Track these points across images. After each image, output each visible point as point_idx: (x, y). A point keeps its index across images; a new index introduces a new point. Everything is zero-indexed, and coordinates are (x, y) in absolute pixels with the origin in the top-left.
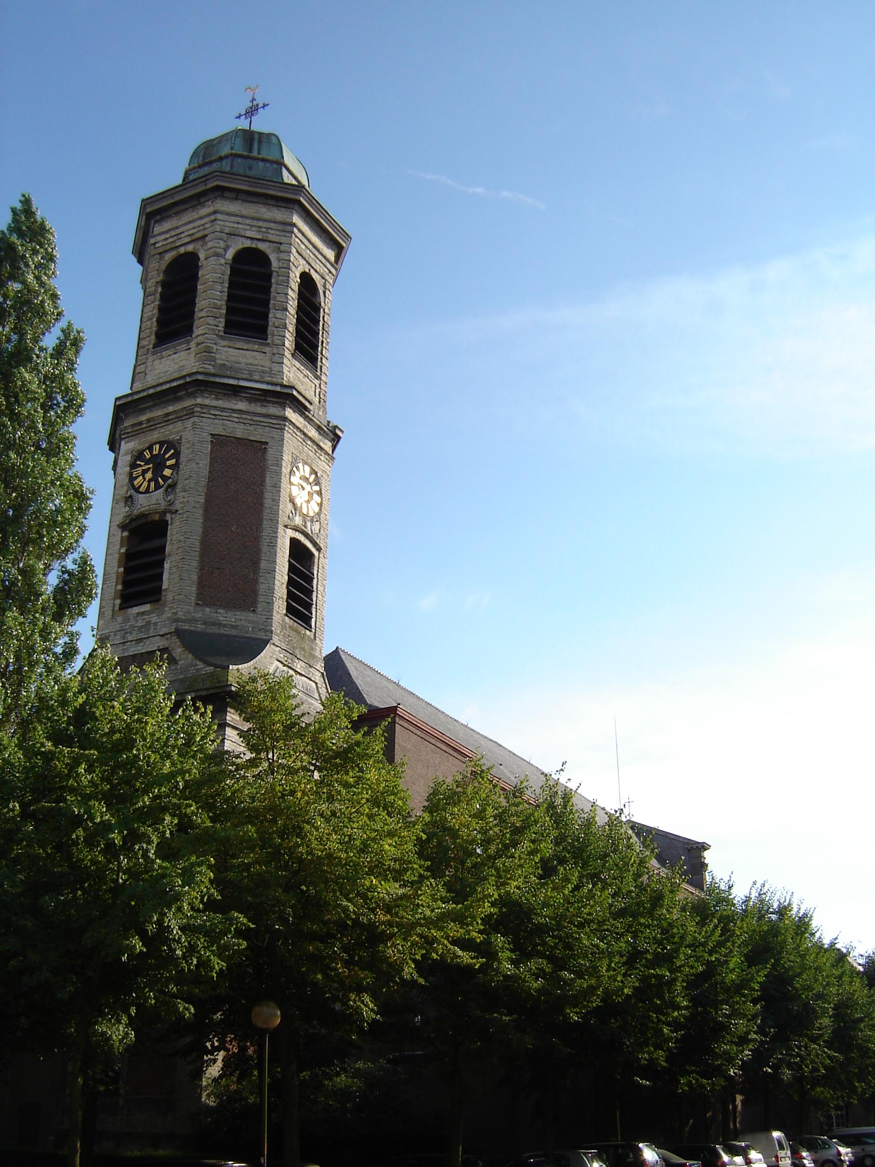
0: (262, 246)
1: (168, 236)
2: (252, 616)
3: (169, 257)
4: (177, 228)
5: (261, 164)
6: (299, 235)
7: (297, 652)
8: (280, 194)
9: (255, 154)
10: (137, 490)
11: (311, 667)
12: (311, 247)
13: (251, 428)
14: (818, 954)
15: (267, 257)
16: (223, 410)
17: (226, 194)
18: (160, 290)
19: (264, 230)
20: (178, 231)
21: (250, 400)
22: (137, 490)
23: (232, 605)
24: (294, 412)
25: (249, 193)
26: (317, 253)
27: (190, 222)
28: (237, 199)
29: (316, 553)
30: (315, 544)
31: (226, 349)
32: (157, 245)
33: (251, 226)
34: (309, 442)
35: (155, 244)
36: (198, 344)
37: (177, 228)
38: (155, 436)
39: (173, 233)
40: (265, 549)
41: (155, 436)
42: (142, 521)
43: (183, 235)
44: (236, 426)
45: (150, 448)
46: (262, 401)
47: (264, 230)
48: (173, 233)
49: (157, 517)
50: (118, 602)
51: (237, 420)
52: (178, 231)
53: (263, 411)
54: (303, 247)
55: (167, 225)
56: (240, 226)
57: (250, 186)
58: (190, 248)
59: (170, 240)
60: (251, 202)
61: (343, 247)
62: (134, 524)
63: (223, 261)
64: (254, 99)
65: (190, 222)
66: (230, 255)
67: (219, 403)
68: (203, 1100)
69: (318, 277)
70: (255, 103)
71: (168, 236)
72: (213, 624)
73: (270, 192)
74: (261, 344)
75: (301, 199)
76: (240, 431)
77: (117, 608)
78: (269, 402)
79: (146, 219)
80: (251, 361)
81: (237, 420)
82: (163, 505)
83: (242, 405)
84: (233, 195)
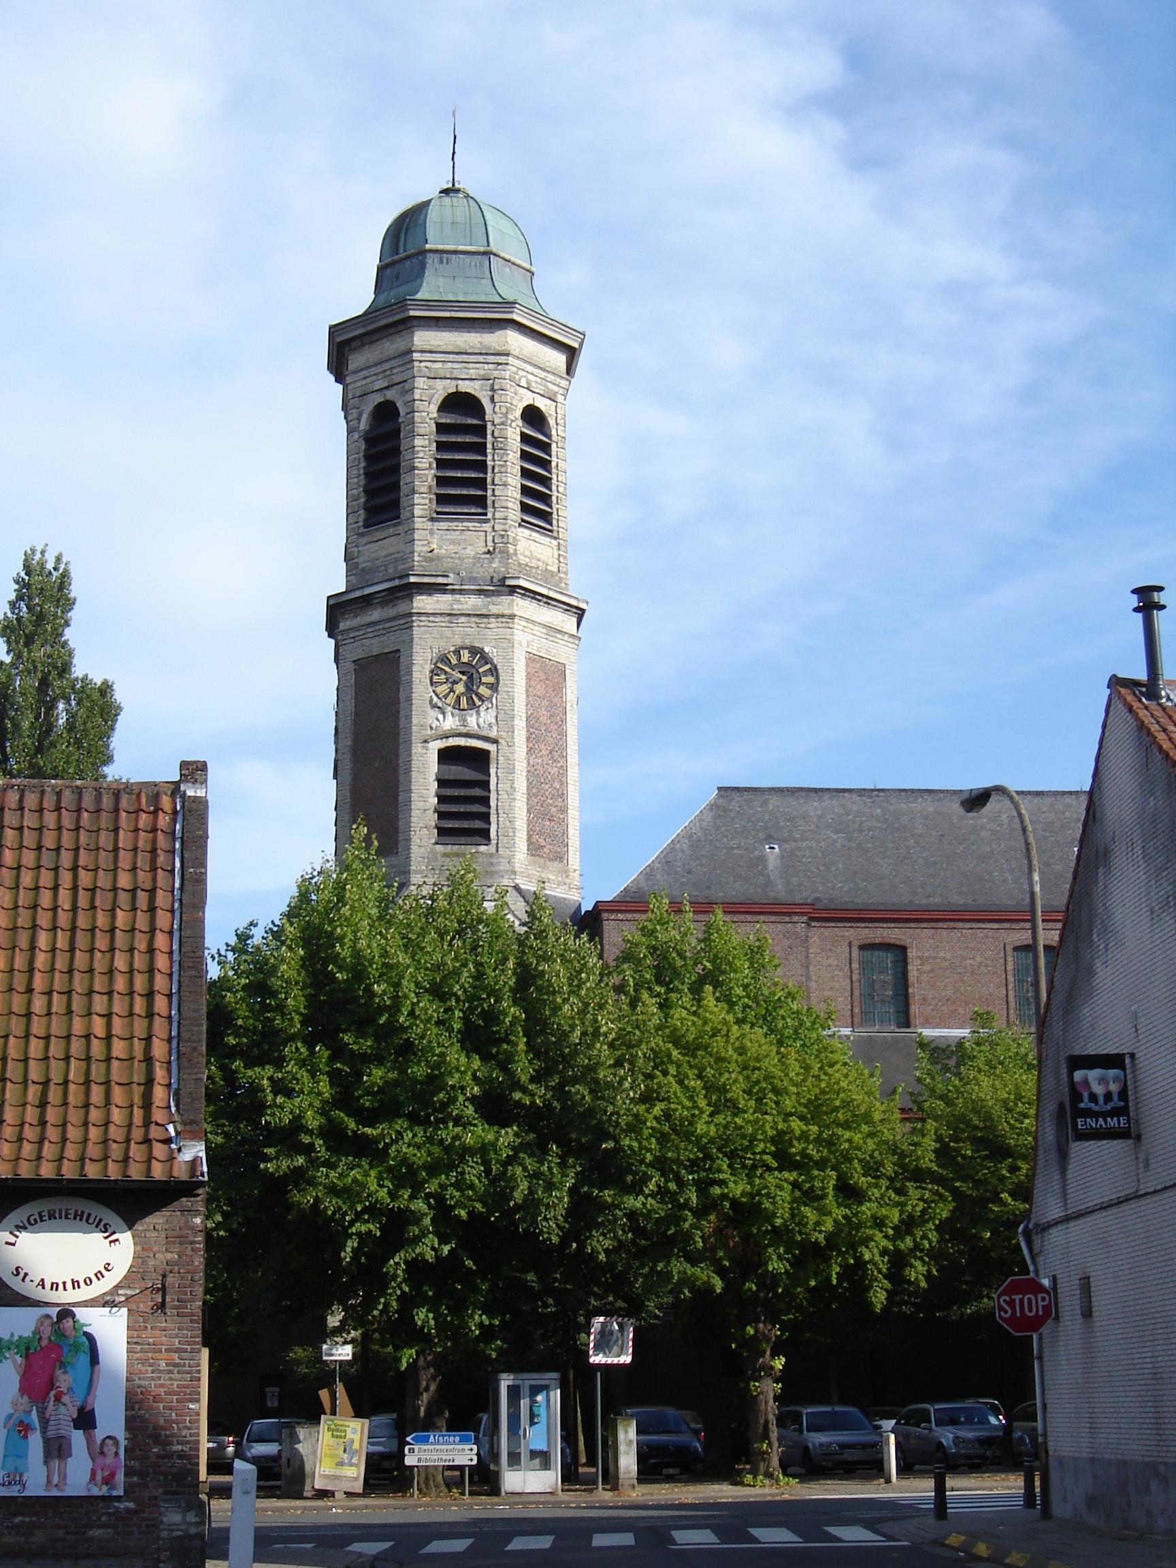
5: (407, 263)
6: (428, 356)
8: (390, 320)
14: (147, 1122)
16: (358, 628)
17: (354, 345)
24: (430, 595)
26: (465, 358)
28: (363, 345)
29: (491, 747)
31: (367, 547)
33: (377, 374)
40: (402, 778)
46: (392, 601)
47: (388, 372)
54: (440, 365)
56: (368, 380)
60: (375, 341)
68: (627, 1359)
73: (382, 323)
74: (395, 525)
75: (412, 313)
78: (398, 598)
80: (391, 550)
83: (375, 615)
84: (358, 343)
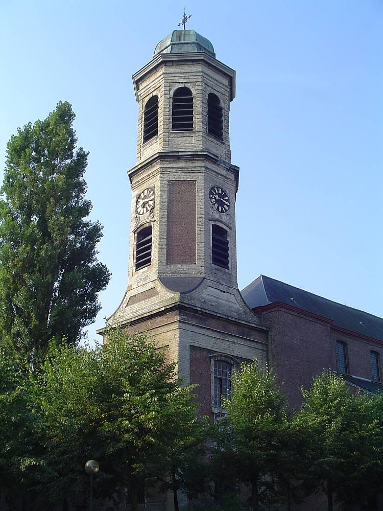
0: (187, 85)
1: (145, 90)
2: (193, 266)
3: (146, 100)
4: (148, 85)
7: (221, 281)
8: (193, 58)
9: (182, 41)
10: (139, 214)
11: (230, 287)
12: (213, 80)
13: (188, 174)
15: (190, 90)
16: (173, 168)
17: (168, 64)
18: (144, 116)
19: (187, 77)
20: (149, 87)
21: (186, 161)
22: (139, 214)
23: (182, 262)
25: (178, 61)
27: (153, 81)
28: (173, 65)
30: (227, 226)
32: (141, 95)
33: (181, 77)
34: (220, 176)
35: (140, 95)
36: (160, 139)
37: (148, 85)
38: (145, 186)
39: (147, 88)
41: (145, 186)
42: (142, 228)
43: (151, 88)
44: (180, 175)
45: (143, 192)
48: (147, 88)
49: (147, 225)
50: (135, 268)
51: (180, 172)
52: (149, 87)
53: (193, 165)
55: (144, 84)
56: (175, 78)
57: (178, 57)
58: (154, 94)
59: (146, 91)
61: (232, 77)
62: (139, 230)
63: (168, 97)
64: (185, 15)
65: (153, 81)
66: (172, 92)
67: (171, 165)
69: (219, 94)
70: (186, 16)
71: (145, 90)
72: (175, 273)
76: (183, 177)
77: (134, 271)
78: (195, 160)
79: (136, 84)
81: (180, 172)
82: (150, 219)
83: (182, 164)
84: (171, 64)
